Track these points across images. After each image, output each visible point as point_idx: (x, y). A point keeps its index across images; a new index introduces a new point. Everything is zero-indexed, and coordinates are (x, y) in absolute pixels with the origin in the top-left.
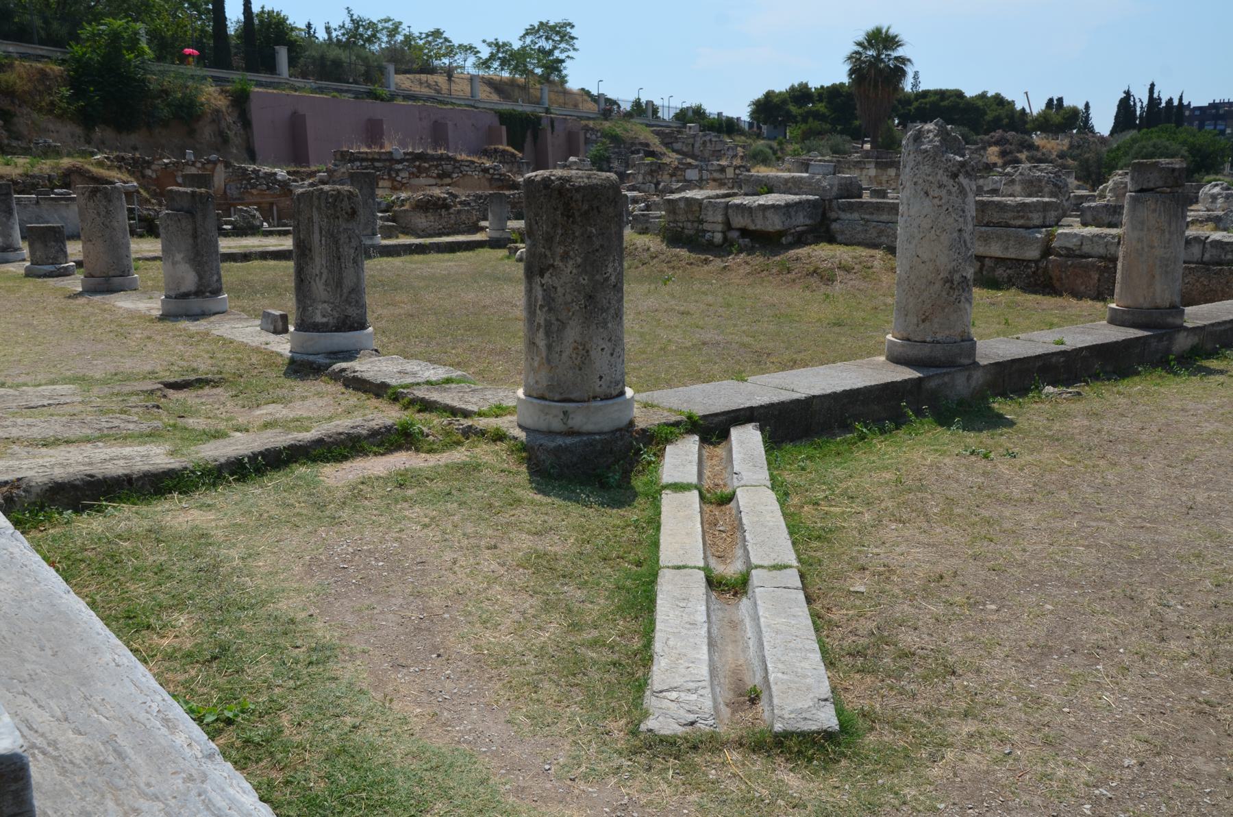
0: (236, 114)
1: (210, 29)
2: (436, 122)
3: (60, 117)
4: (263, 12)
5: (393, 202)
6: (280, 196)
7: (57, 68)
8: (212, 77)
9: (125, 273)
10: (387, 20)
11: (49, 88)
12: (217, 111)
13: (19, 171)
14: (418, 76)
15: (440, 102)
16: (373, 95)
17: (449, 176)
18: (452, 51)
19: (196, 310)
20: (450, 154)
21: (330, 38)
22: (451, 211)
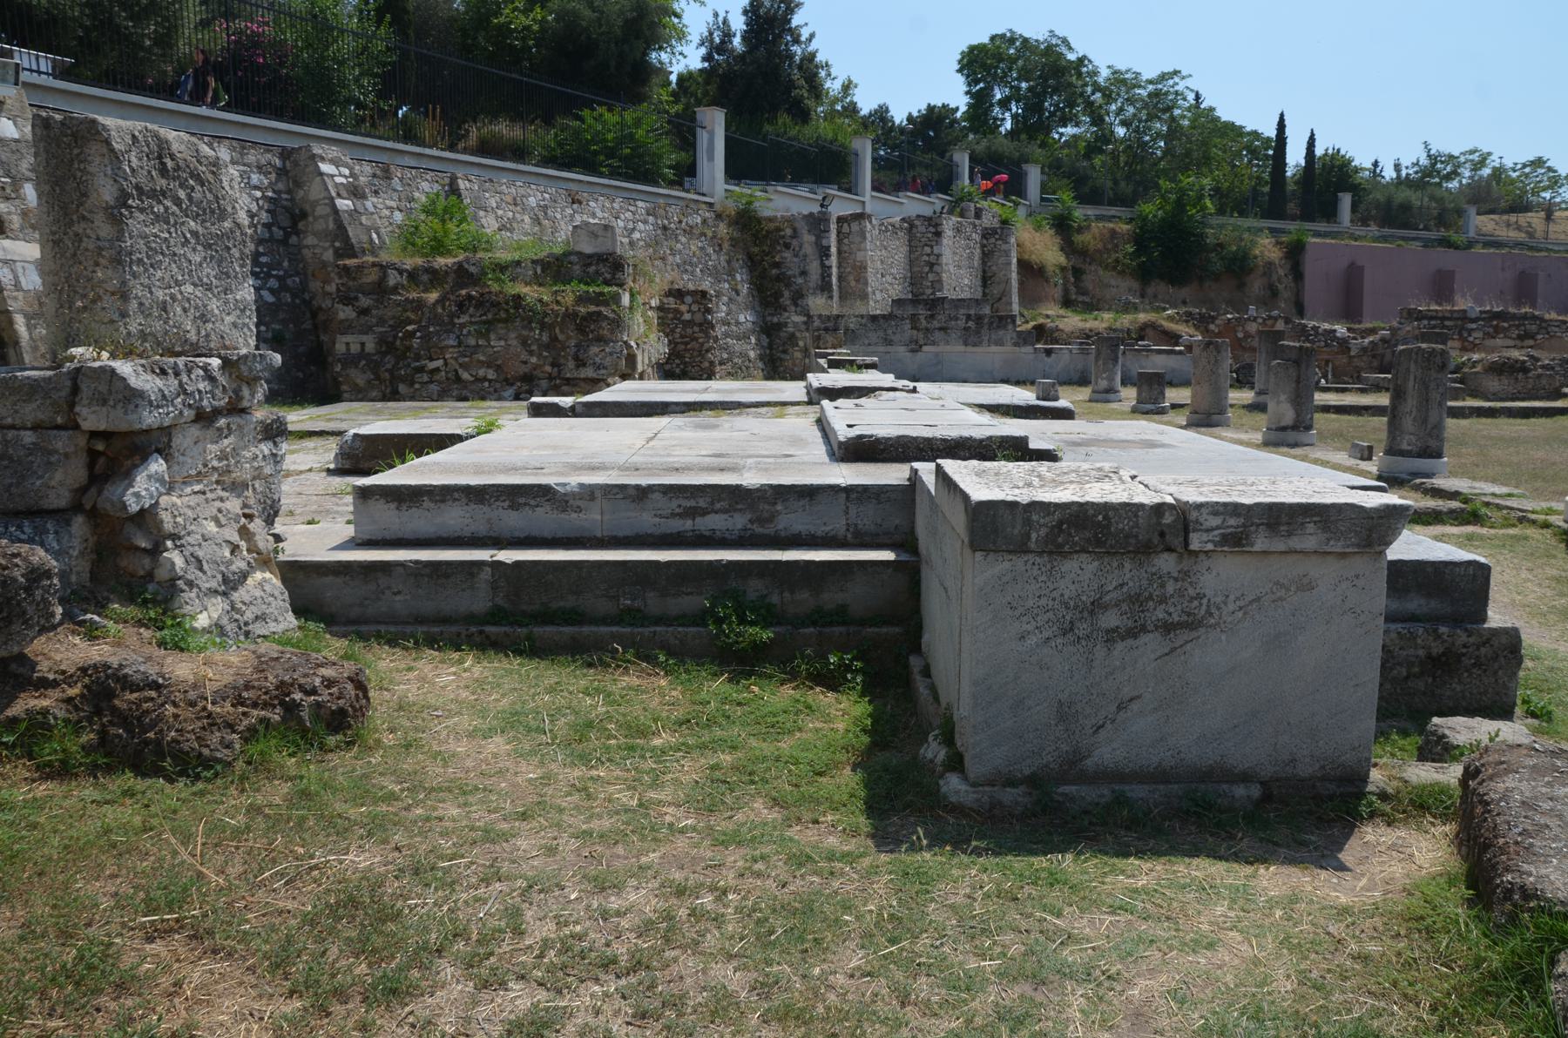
0: (1288, 266)
1: (1266, 176)
2: (1523, 272)
3: (1122, 273)
4: (1326, 154)
5: (1463, 363)
6: (1337, 353)
7: (1125, 227)
8: (1269, 228)
9: (1222, 412)
10: (1472, 152)
11: (1117, 246)
12: (1270, 264)
13: (1104, 325)
14: (1505, 217)
15: (1531, 248)
16: (1446, 243)
17: (1533, 337)
18: (1556, 182)
19: (1291, 441)
20: (1537, 313)
21: (1399, 176)
22: (1530, 375)
